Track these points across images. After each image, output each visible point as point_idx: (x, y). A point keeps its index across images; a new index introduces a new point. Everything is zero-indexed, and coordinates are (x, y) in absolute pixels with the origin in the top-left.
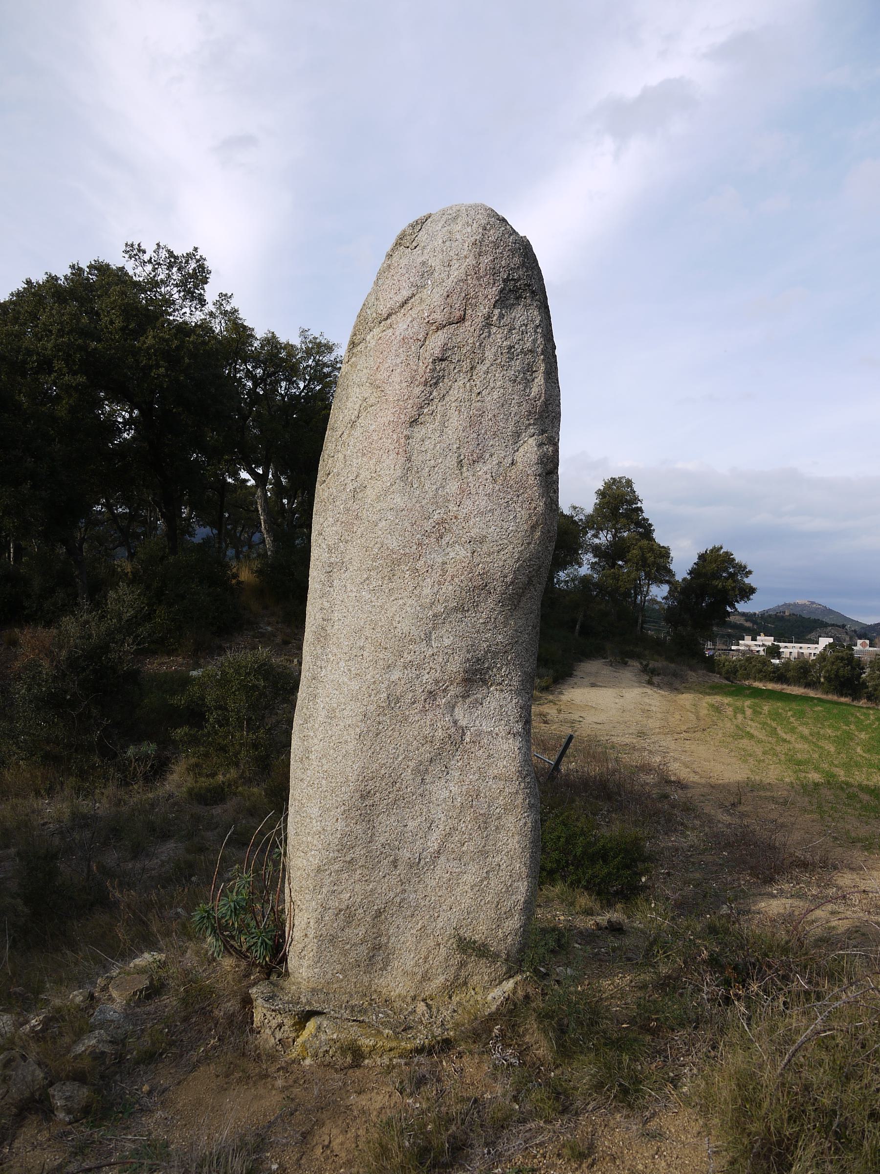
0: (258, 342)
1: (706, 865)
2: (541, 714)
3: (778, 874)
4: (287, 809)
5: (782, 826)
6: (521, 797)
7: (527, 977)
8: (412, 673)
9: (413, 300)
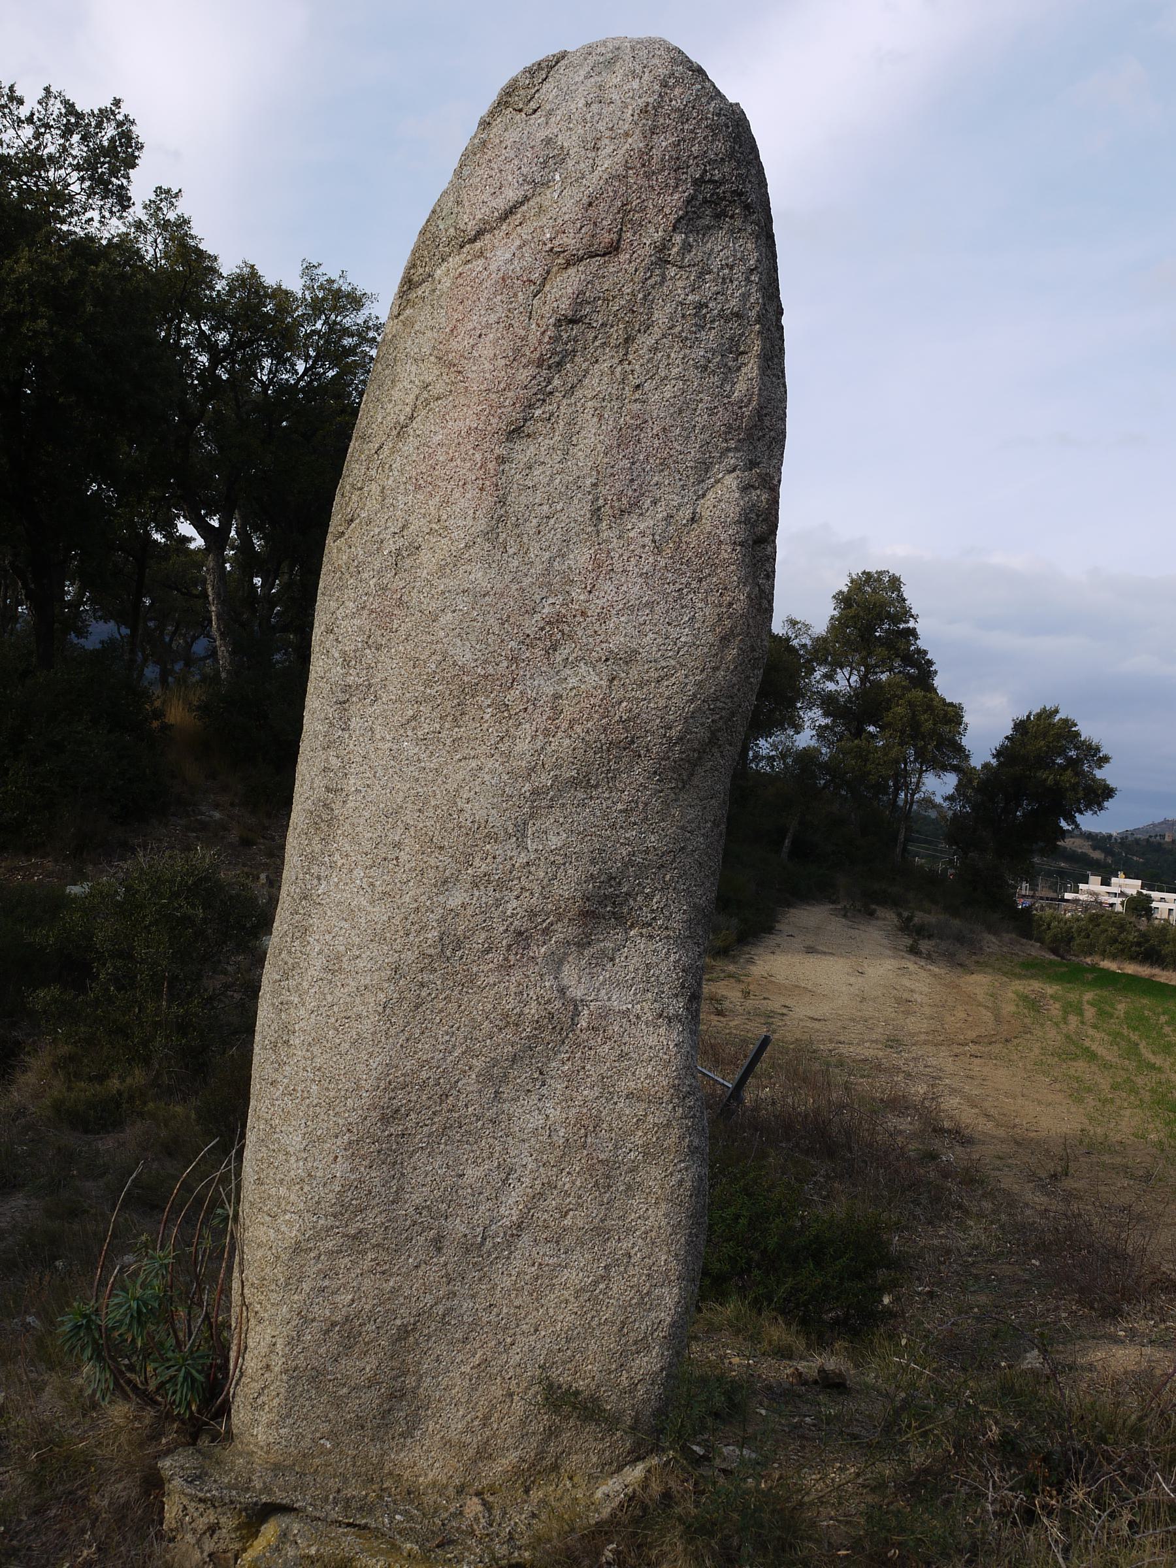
0: (224, 282)
1: (1000, 1280)
2: (713, 998)
3: (1129, 1303)
4: (243, 1136)
5: (1140, 1218)
6: (676, 1132)
7: (669, 1461)
8: (486, 896)
9: (524, 208)
